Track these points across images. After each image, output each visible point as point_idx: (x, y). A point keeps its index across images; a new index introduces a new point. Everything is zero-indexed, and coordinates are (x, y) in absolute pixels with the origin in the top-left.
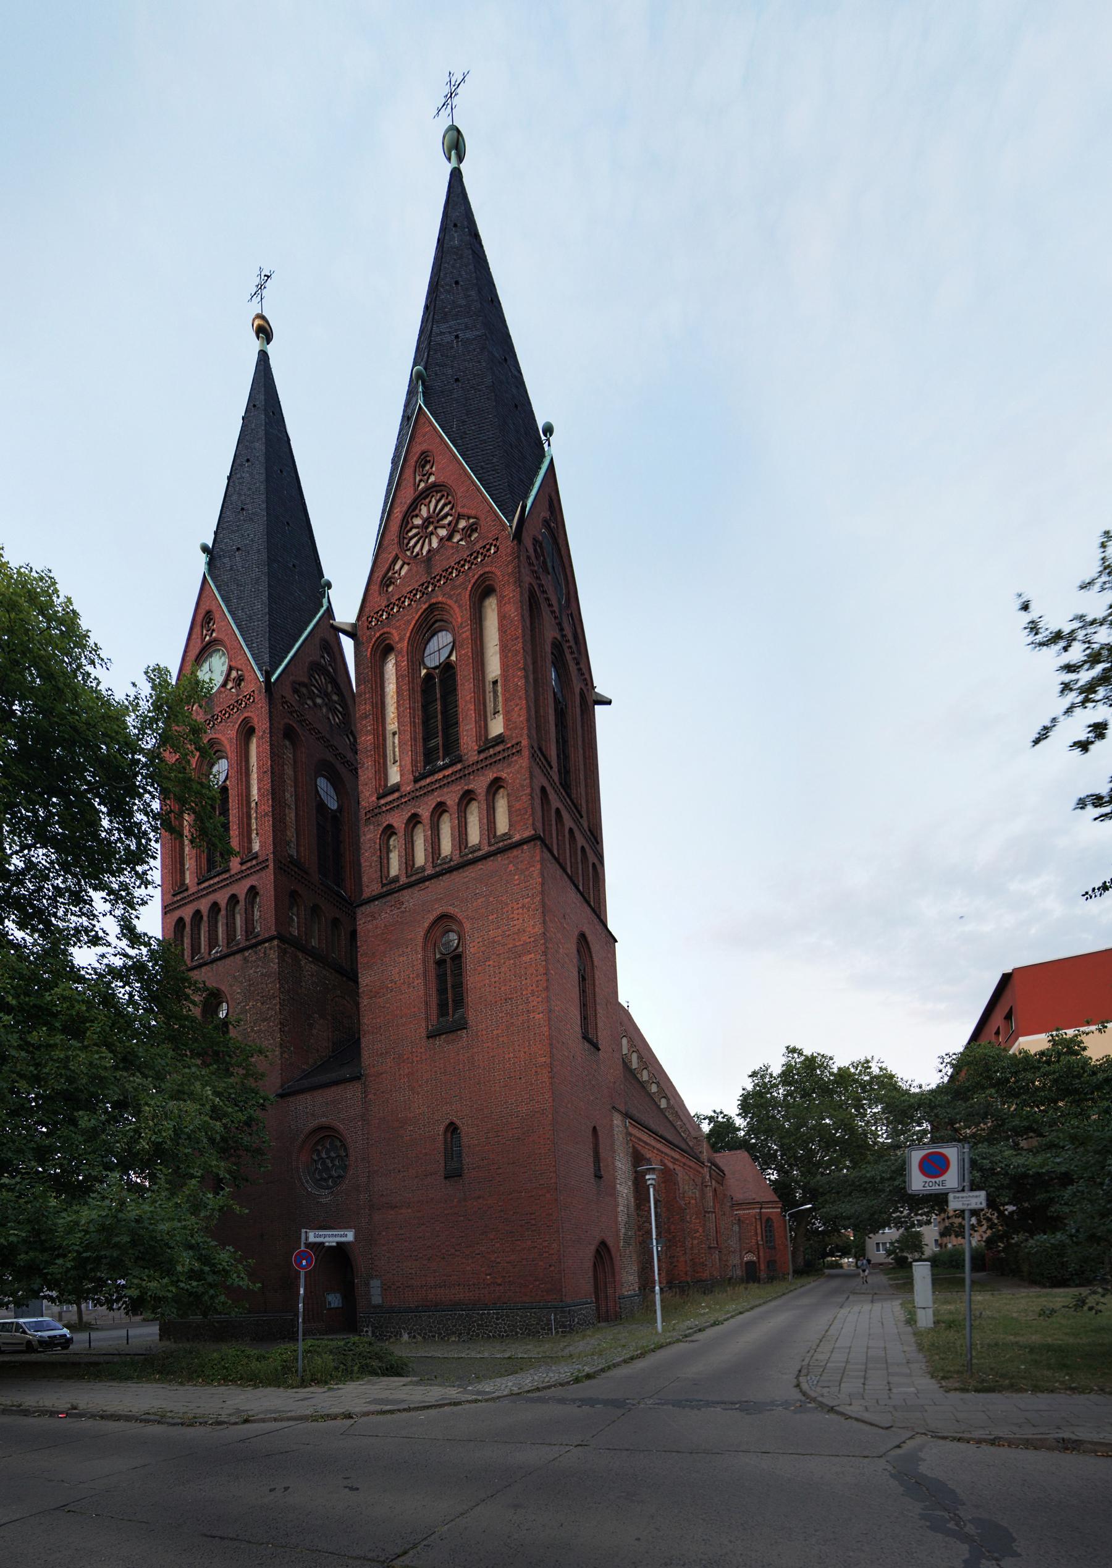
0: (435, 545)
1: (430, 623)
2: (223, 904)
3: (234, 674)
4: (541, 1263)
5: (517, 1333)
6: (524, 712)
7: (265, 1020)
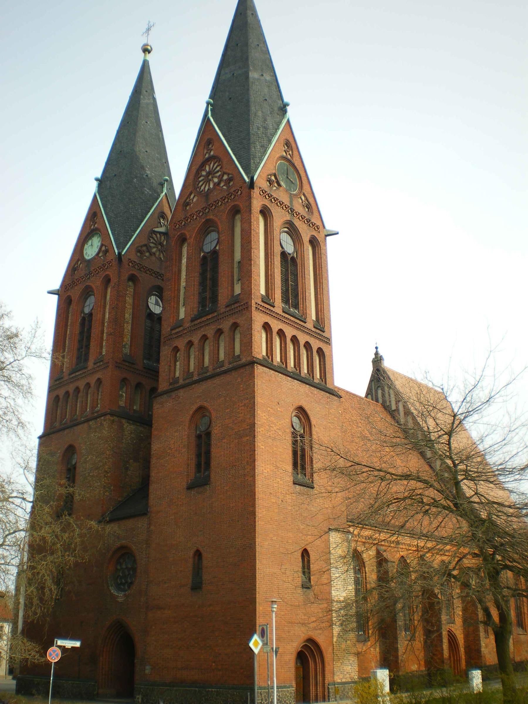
0: (211, 186)
1: (209, 226)
3: (103, 248)
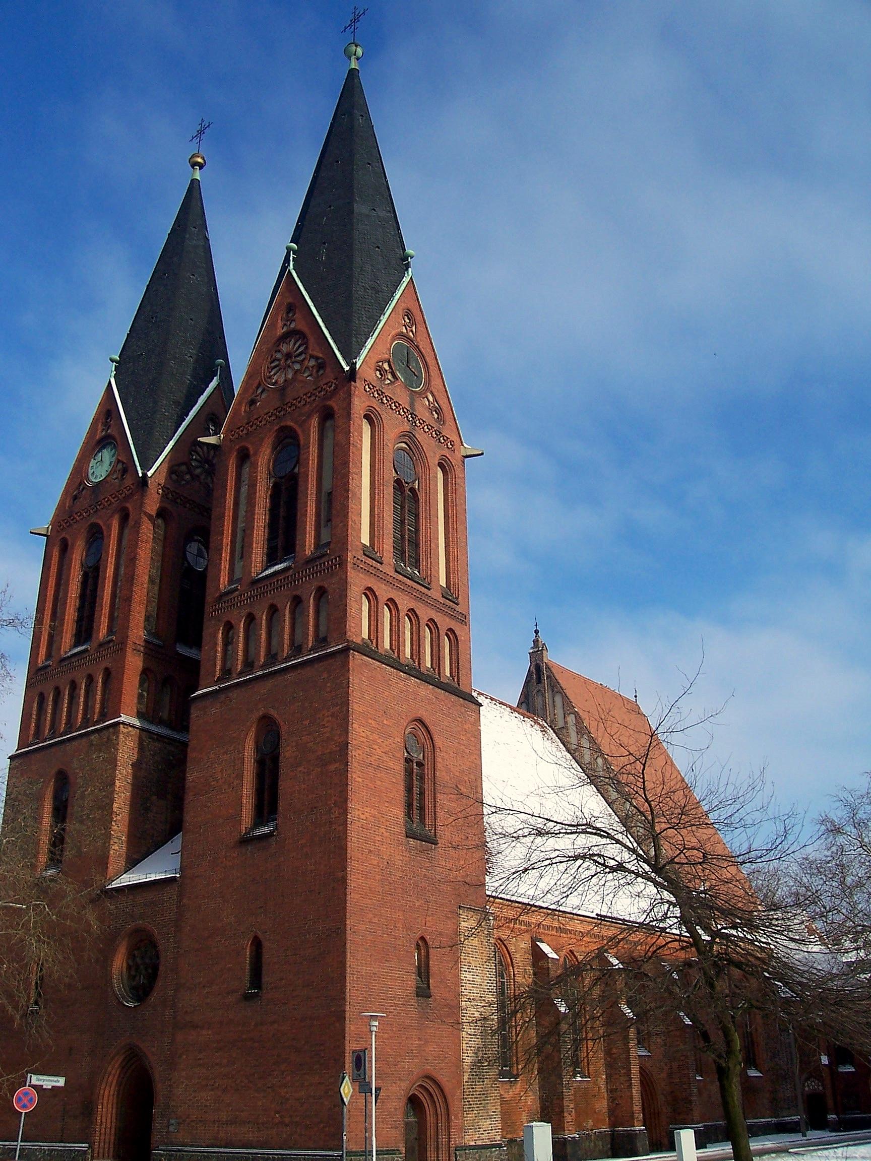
7: (99, 808)
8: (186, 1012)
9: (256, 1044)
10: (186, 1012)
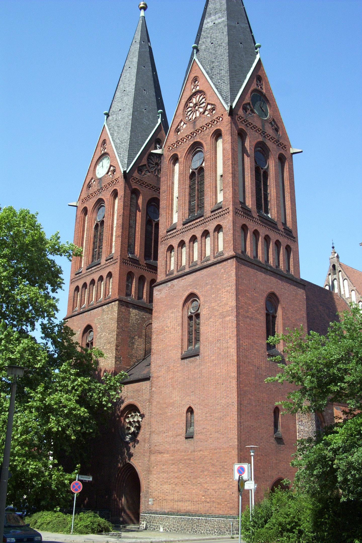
2: (96, 280)
3: (112, 168)
4: (228, 491)
5: (215, 532)
6: (231, 194)
7: (109, 343)
8: (156, 445)
9: (192, 462)
10: (156, 445)
